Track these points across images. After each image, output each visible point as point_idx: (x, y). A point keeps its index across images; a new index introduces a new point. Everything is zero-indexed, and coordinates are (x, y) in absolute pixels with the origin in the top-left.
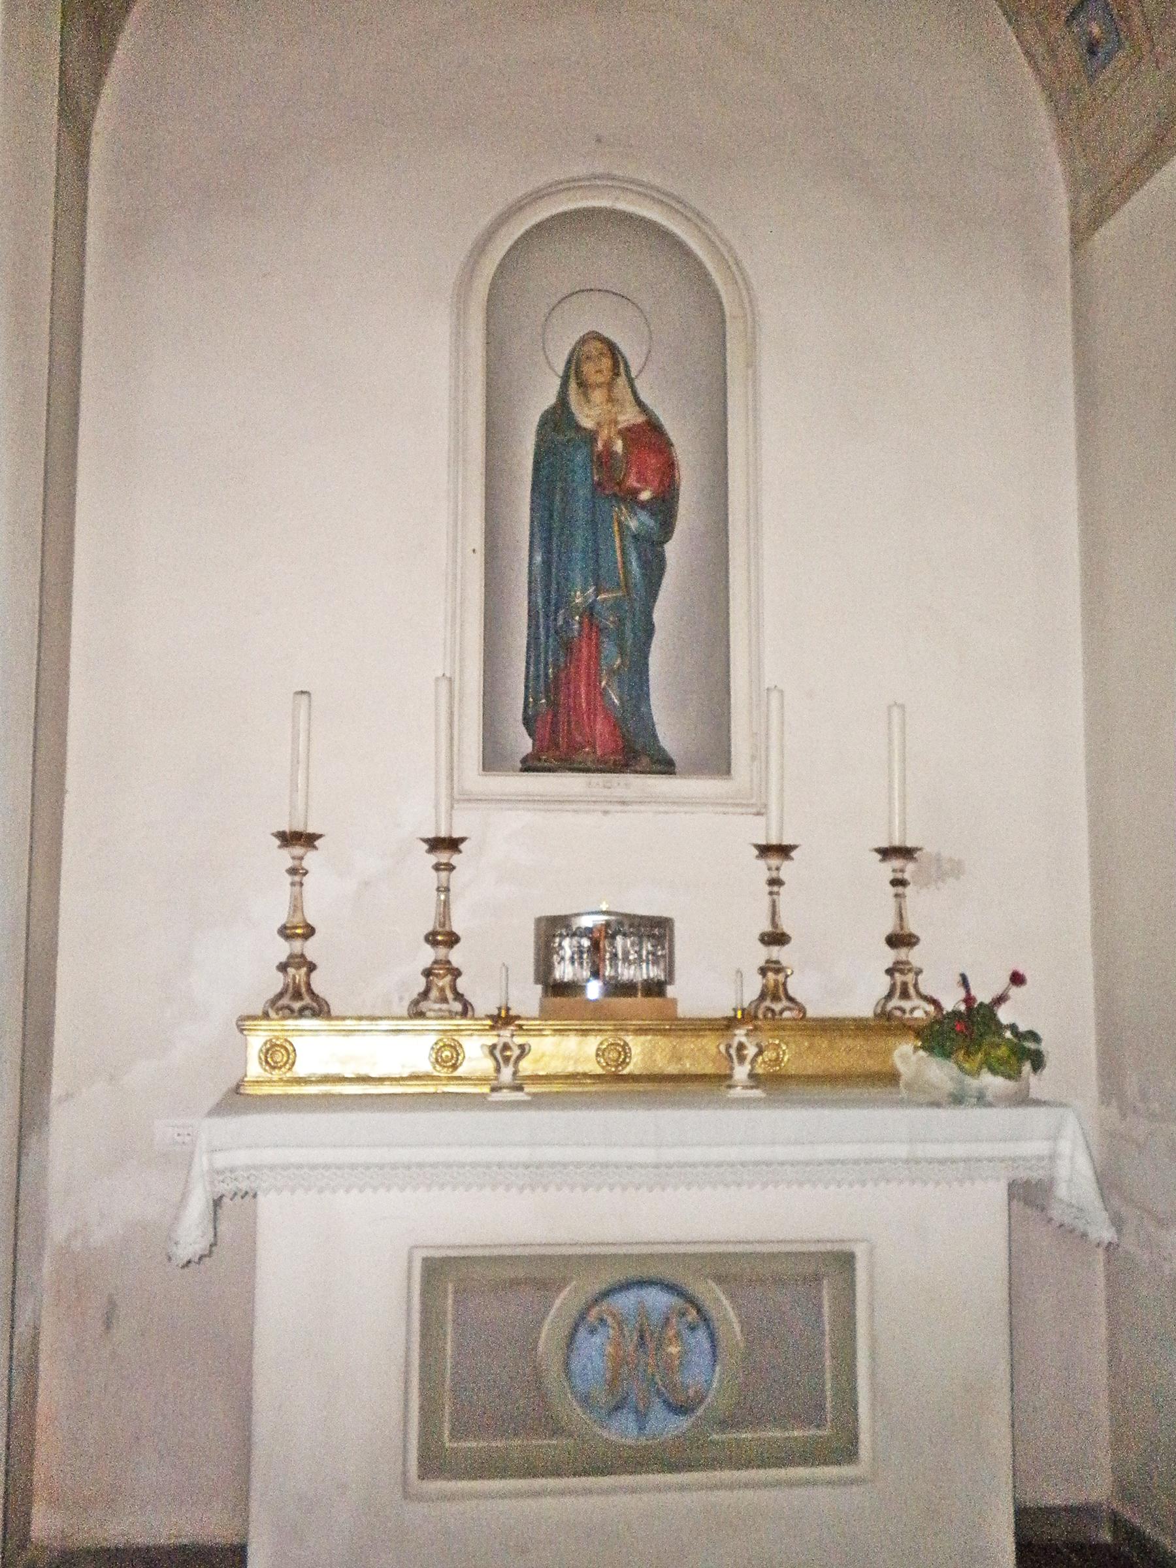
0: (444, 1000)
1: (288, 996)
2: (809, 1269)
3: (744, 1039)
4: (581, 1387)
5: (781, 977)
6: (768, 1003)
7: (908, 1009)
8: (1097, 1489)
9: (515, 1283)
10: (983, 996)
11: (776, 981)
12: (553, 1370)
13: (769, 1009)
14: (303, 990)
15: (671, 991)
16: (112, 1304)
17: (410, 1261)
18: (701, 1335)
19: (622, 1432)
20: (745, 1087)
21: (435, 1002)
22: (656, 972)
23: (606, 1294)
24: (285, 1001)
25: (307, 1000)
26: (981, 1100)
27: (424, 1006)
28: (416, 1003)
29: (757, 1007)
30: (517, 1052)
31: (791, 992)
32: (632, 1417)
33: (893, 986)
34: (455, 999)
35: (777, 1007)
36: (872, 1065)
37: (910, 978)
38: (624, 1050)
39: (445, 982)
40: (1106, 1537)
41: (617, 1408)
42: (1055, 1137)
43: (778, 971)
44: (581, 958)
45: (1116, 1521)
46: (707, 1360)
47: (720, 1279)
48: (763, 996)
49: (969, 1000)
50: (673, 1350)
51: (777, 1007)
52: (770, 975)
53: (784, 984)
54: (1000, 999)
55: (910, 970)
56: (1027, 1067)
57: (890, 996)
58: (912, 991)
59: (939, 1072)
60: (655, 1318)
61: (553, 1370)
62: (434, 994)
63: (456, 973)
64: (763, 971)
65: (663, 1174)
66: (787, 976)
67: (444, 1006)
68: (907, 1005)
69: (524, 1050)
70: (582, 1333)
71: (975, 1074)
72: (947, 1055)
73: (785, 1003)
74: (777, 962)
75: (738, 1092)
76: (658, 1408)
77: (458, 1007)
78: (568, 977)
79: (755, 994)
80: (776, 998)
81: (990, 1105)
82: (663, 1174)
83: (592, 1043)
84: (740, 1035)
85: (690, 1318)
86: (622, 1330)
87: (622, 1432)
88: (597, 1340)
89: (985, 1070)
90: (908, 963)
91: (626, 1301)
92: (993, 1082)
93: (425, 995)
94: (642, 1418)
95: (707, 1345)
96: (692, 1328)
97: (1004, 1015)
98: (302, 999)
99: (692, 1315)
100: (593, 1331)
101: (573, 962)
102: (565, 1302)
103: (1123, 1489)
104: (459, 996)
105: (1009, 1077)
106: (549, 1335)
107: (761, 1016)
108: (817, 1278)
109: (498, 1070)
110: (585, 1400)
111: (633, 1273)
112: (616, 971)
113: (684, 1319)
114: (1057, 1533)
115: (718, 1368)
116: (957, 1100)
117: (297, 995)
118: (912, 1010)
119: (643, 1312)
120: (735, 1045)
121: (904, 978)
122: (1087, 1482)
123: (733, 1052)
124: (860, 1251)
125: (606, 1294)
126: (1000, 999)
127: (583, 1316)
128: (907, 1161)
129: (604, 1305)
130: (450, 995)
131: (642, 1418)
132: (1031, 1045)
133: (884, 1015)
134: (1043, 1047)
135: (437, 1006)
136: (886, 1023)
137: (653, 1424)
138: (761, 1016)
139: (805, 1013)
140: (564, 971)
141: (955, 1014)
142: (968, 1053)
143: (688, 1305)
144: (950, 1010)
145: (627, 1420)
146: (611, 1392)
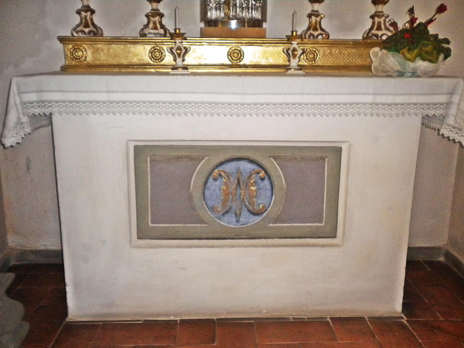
0: (156, 28)
1: (83, 25)
2: (319, 154)
3: (296, 46)
4: (210, 204)
5: (318, 19)
6: (311, 31)
7: (380, 35)
8: (441, 241)
9: (179, 158)
10: (421, 19)
11: (316, 21)
12: (197, 195)
13: (311, 34)
14: (90, 22)
15: (265, 25)
16: (28, 160)
17: (127, 147)
18: (266, 182)
19: (229, 222)
20: (295, 69)
21: (152, 29)
22: (257, 15)
23: (222, 163)
24: (81, 28)
25: (92, 28)
26: (414, 74)
27: (146, 31)
28: (142, 30)
29: (306, 33)
30: (184, 51)
31: (323, 27)
32: (233, 216)
33: (373, 23)
34: (161, 28)
35: (316, 33)
36: (359, 62)
37: (382, 20)
38: (240, 52)
39: (157, 19)
40: (442, 259)
41: (227, 212)
42: (452, 93)
43: (317, 16)
44: (220, 7)
45: (448, 255)
46: (269, 193)
47: (275, 158)
48: (309, 29)
49: (413, 20)
50: (253, 188)
51: (316, 33)
52: (313, 18)
53: (320, 23)
54: (430, 21)
55: (383, 16)
56: (442, 57)
57: (372, 28)
58: (383, 26)
59: (392, 60)
60: (245, 175)
61: (197, 195)
62: (151, 25)
63: (162, 15)
64: (310, 16)
65: (243, 109)
66: (322, 18)
67: (156, 31)
68: (380, 33)
69: (187, 50)
70: (211, 180)
71: (413, 60)
72: (398, 51)
73: (319, 32)
74: (317, 11)
75: (292, 71)
76: (245, 213)
77: (162, 31)
78: (214, 17)
79: (305, 27)
80: (315, 29)
81: (419, 76)
82: (243, 109)
83: (225, 50)
84: (295, 44)
85: (261, 174)
86: (229, 178)
87: (229, 222)
88: (218, 183)
89: (419, 58)
90: (382, 12)
91: (230, 167)
92: (422, 65)
93: (146, 26)
94: (238, 216)
95: (269, 187)
96: (262, 179)
97: (432, 30)
98: (89, 27)
99: (262, 174)
100: (215, 180)
101: (216, 10)
102: (202, 167)
103: (452, 241)
104: (162, 27)
105: (430, 61)
106: (195, 181)
107: (307, 37)
108: (323, 159)
109: (175, 60)
110: (212, 209)
111: (228, 155)
112: (236, 12)
113: (259, 175)
114: (421, 257)
115: (274, 196)
116: (401, 74)
117: (87, 26)
118: (382, 36)
119: (238, 171)
120: (291, 49)
121: (380, 20)
122: (437, 238)
123: (290, 52)
124: (344, 147)
125: (222, 163)
126: (430, 21)
127: (210, 174)
128: (371, 104)
129: (220, 168)
130: (158, 26)
131: (238, 216)
132: (446, 46)
133: (368, 36)
134: (451, 46)
135: (152, 31)
136: (368, 41)
137: (242, 219)
138: (307, 37)
139: (329, 37)
140: (213, 14)
141: (404, 31)
142: (409, 50)
143: (260, 169)
144: (401, 29)
145: (231, 218)
146: (224, 205)
